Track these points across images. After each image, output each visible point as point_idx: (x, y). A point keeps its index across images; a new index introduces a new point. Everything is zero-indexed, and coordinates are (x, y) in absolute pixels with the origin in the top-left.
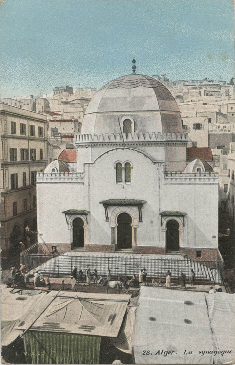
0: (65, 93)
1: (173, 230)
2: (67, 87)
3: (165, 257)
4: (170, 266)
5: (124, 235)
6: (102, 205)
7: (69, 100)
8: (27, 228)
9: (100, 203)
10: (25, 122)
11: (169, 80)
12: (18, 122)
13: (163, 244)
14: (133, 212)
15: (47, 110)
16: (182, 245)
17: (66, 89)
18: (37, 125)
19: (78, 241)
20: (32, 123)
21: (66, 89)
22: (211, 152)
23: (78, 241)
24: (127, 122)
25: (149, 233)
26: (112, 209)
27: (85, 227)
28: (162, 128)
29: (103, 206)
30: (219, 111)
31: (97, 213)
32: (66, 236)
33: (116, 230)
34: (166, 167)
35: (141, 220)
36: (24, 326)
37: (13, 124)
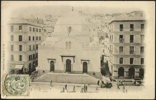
3: (82, 75)
5: (68, 69)
10: (34, 27)
11: (12, 46)
12: (32, 27)
13: (82, 70)
14: (71, 59)
15: (43, 23)
16: (88, 70)
18: (39, 28)
19: (52, 69)
20: (37, 27)
23: (52, 69)
25: (77, 66)
26: (64, 58)
28: (66, 68)
31: (59, 59)
33: (65, 65)
34: (75, 87)
37: (30, 28)
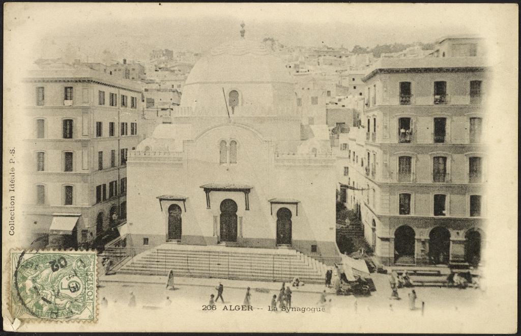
0: (163, 58)
1: (284, 216)
2: (166, 50)
3: (273, 251)
4: (282, 261)
5: (229, 231)
6: (203, 189)
7: (168, 66)
8: (114, 215)
9: (200, 187)
10: (113, 90)
12: (108, 91)
14: (239, 198)
16: (295, 237)
17: (164, 53)
18: (129, 95)
19: (175, 231)
20: (123, 92)
21: (164, 53)
22: (465, 278)
23: (175, 231)
24: (234, 93)
25: (257, 223)
27: (184, 216)
29: (205, 190)
30: (339, 83)
32: (161, 226)
35: (247, 209)
36: (169, 206)
37: (102, 93)
